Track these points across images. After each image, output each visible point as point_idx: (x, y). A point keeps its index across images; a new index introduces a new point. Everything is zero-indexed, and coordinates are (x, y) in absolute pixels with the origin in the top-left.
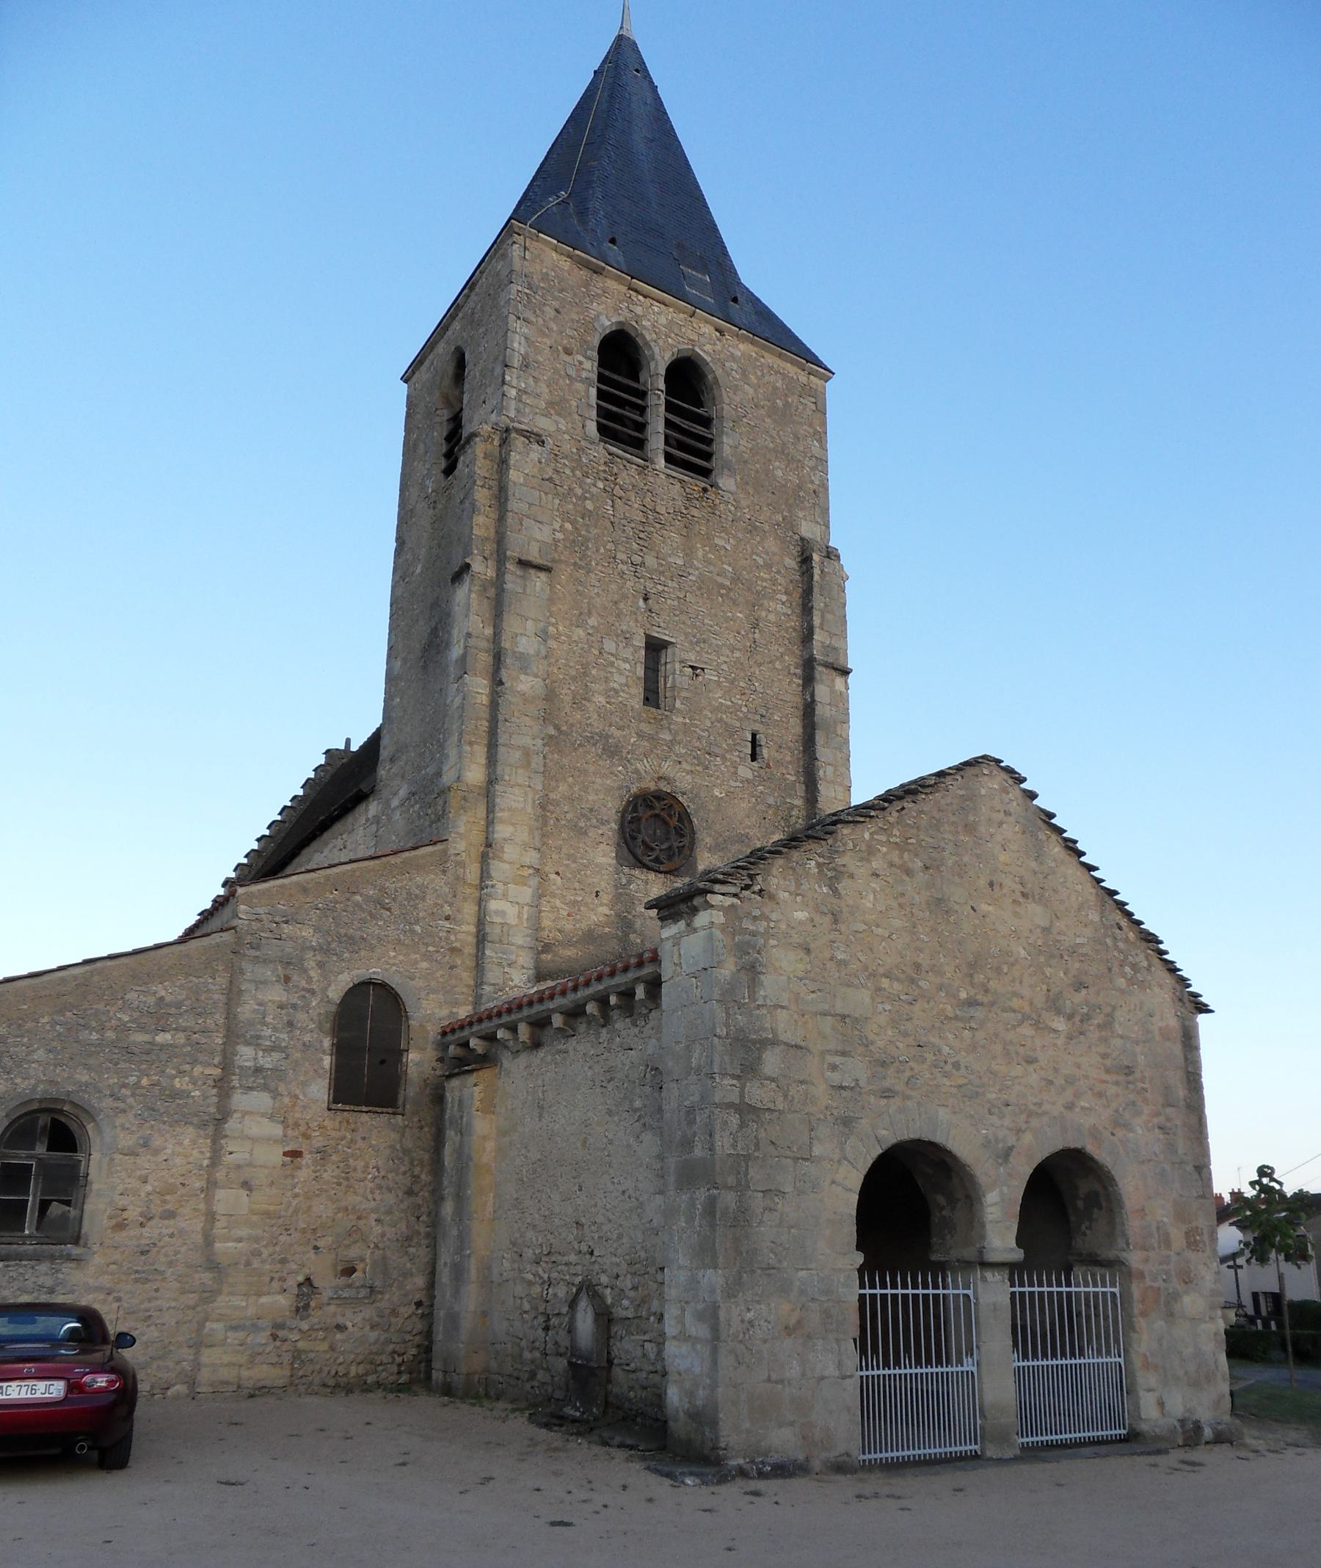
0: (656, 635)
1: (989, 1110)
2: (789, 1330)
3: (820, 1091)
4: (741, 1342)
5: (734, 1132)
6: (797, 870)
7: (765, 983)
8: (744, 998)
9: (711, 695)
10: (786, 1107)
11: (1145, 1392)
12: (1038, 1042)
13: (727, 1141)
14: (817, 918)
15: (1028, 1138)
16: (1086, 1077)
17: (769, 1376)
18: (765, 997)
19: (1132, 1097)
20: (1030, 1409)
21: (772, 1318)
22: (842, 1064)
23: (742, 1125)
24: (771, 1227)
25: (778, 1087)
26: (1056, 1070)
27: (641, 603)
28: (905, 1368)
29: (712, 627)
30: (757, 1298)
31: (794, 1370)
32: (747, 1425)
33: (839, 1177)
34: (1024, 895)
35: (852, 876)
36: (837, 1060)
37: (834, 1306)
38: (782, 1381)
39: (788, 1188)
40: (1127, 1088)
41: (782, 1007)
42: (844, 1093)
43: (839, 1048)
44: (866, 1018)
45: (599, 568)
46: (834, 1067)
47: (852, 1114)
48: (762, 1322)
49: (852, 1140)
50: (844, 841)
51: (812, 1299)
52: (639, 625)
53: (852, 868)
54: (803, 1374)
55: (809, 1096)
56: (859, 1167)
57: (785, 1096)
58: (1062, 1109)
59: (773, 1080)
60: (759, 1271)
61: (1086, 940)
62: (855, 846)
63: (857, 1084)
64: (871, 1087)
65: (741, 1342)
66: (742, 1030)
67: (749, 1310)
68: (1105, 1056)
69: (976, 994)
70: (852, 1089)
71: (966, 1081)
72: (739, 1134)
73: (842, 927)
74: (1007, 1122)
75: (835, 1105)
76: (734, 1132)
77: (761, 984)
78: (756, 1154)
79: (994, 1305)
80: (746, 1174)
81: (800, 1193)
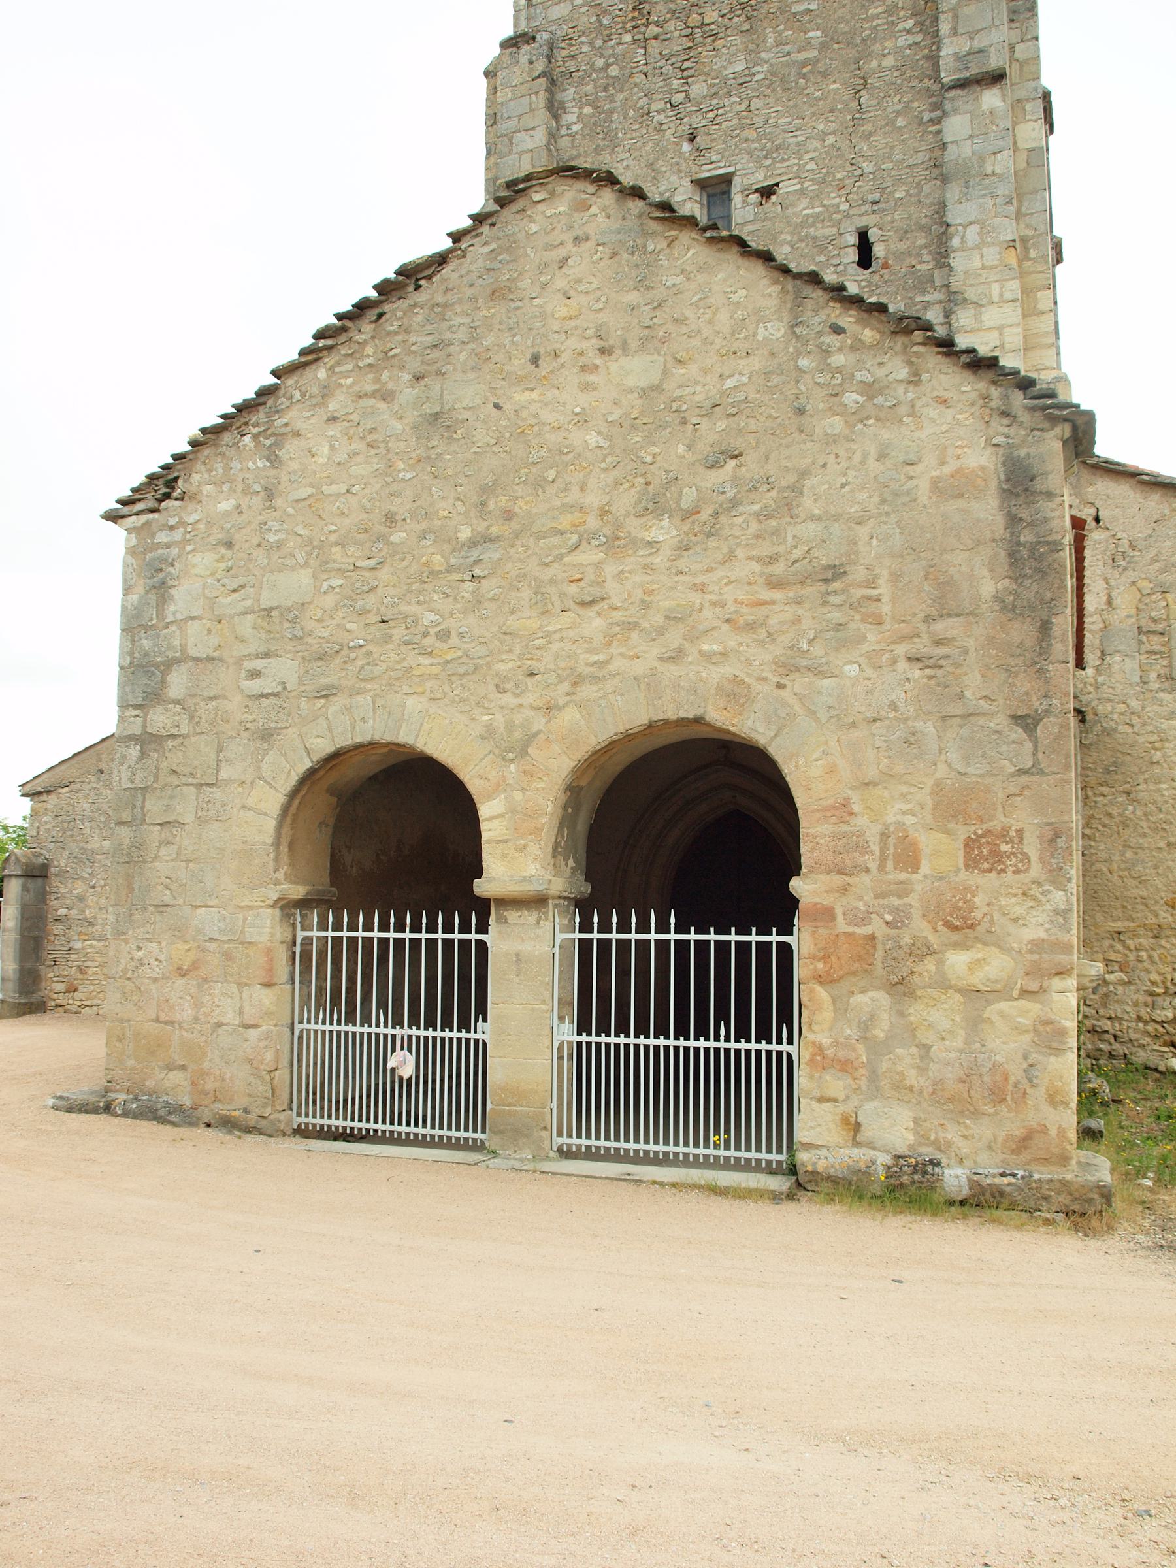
0: (707, 175)
1: (497, 686)
2: (182, 973)
3: (234, 705)
4: (129, 979)
5: (132, 764)
6: (228, 453)
7: (176, 597)
8: (151, 620)
9: (790, 211)
10: (192, 729)
11: (814, 1104)
12: (610, 570)
13: (125, 775)
14: (245, 502)
15: (570, 716)
16: (719, 604)
17: (158, 1016)
18: (174, 614)
19: (837, 616)
20: (434, 1090)
21: (162, 957)
22: (265, 667)
23: (143, 754)
24: (167, 861)
25: (183, 708)
26: (645, 605)
27: (686, 147)
28: (378, 1026)
29: (790, 124)
30: (148, 936)
31: (186, 1013)
32: (132, 1062)
33: (250, 802)
34: (603, 351)
35: (297, 434)
36: (258, 664)
37: (236, 948)
38: (171, 1023)
39: (189, 818)
40: (825, 603)
41: (193, 618)
42: (265, 702)
43: (261, 650)
44: (303, 604)
45: (629, 136)
46: (254, 674)
47: (273, 725)
48: (152, 961)
49: (271, 757)
50: (288, 395)
51: (210, 938)
52: (683, 175)
53: (299, 425)
54: (196, 1019)
55: (220, 713)
56: (278, 786)
57: (192, 718)
58: (656, 664)
59: (178, 702)
60: (151, 909)
61: (745, 379)
62: (303, 395)
63: (285, 688)
64: (303, 688)
65: (129, 979)
66: (147, 654)
67: (139, 948)
68: (772, 559)
69: (488, 528)
70: (276, 695)
71: (460, 653)
72: (137, 766)
73: (279, 502)
74: (530, 698)
75: (251, 718)
76: (132, 764)
77: (172, 599)
78: (155, 785)
79: (517, 955)
80: (143, 808)
81: (201, 821)
